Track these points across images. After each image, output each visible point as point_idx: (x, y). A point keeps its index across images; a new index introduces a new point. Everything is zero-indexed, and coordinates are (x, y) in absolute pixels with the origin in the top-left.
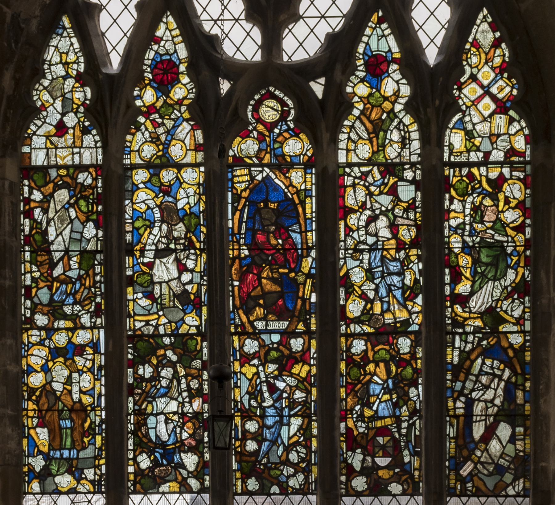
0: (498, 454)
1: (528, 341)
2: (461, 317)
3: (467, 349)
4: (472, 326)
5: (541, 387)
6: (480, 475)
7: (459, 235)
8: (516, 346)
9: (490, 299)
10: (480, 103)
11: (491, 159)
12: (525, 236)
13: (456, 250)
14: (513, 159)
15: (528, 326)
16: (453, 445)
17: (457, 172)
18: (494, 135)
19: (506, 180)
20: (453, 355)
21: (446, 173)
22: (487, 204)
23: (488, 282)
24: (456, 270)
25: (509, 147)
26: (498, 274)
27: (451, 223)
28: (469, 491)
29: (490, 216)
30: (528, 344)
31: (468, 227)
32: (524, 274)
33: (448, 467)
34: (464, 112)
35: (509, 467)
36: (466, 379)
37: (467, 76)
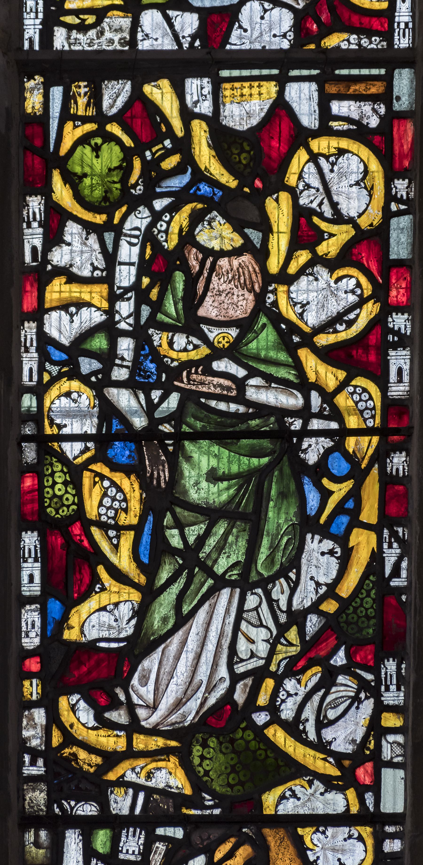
2: (91, 749)
4: (137, 788)
7: (85, 380)
9: (223, 672)
13: (72, 449)
14: (333, 41)
15: (394, 793)
17: (82, 101)
19: (301, 137)
21: (33, 102)
22: (216, 245)
23: (213, 592)
24: (68, 537)
29: (226, 300)
31: (125, 346)
32: (377, 558)
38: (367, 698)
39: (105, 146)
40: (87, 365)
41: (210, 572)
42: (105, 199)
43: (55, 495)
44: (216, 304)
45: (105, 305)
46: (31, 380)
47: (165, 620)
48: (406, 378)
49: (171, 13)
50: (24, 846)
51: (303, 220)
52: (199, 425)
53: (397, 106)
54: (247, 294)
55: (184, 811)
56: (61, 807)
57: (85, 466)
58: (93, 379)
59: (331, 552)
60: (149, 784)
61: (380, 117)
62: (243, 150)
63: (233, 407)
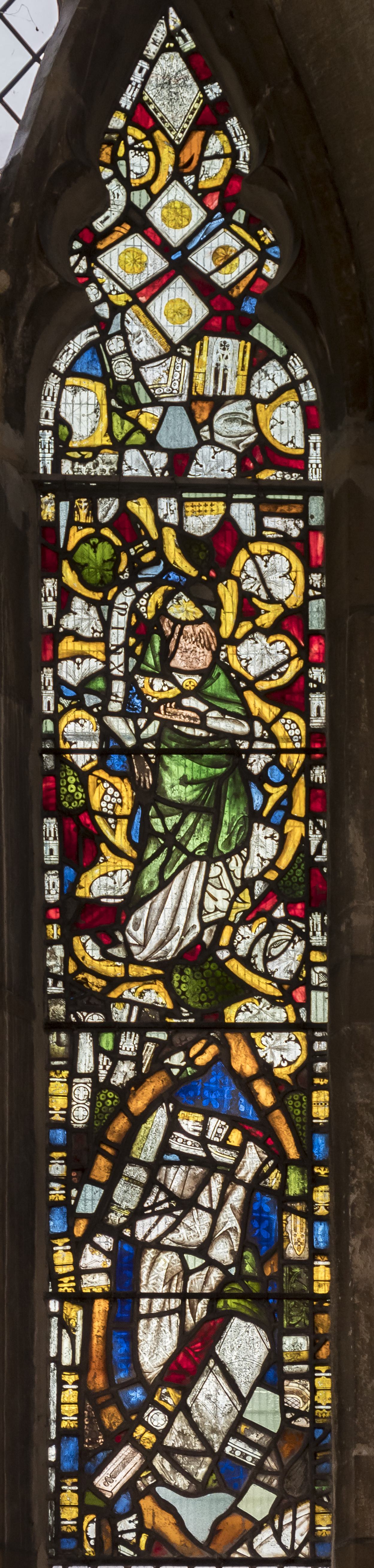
0: (224, 1424)
1: (321, 1057)
2: (98, 975)
3: (118, 1080)
4: (133, 1003)
5: (353, 1197)
6: (162, 1491)
7: (89, 710)
8: (283, 1073)
9: (195, 921)
10: (157, 301)
11: (194, 472)
12: (307, 720)
13: (80, 760)
14: (264, 475)
15: (320, 1009)
16: (70, 1395)
17: (83, 512)
18: (203, 398)
19: (243, 542)
20: (69, 1097)
21: (48, 512)
22: (182, 616)
23: (186, 864)
25: (251, 439)
26: (223, 836)
27: (63, 674)
28: (126, 1543)
29: (191, 655)
30: (320, 1066)
31: (118, 687)
32: (305, 841)
33: (56, 1465)
34: (104, 325)
35: (260, 1467)
36: (116, 1175)
37: (113, 214)
38: (300, 940)
39: (100, 545)
40: (91, 700)
41: (184, 850)
42: (102, 582)
43: (68, 793)
44: (184, 658)
45: (102, 657)
46: (49, 709)
47: (151, 883)
48: (323, 713)
49: (147, 452)
50: (49, 1044)
51: (245, 600)
52: (174, 744)
53: (313, 522)
54: (206, 651)
55: (168, 1020)
56: (76, 1016)
57: (90, 772)
58: (95, 710)
59: (272, 837)
60: (141, 1000)
61: (300, 530)
62: (201, 550)
63: (198, 732)
